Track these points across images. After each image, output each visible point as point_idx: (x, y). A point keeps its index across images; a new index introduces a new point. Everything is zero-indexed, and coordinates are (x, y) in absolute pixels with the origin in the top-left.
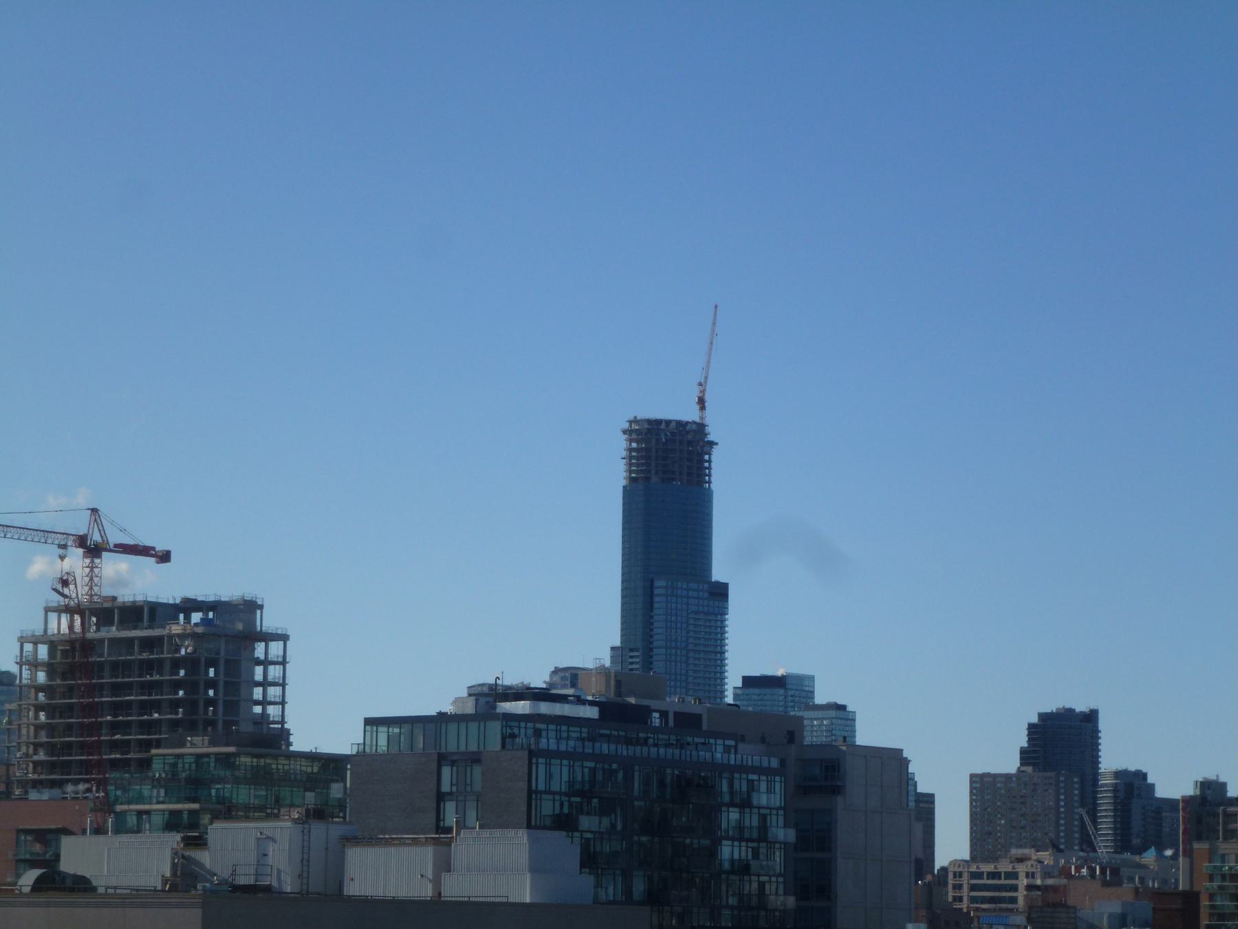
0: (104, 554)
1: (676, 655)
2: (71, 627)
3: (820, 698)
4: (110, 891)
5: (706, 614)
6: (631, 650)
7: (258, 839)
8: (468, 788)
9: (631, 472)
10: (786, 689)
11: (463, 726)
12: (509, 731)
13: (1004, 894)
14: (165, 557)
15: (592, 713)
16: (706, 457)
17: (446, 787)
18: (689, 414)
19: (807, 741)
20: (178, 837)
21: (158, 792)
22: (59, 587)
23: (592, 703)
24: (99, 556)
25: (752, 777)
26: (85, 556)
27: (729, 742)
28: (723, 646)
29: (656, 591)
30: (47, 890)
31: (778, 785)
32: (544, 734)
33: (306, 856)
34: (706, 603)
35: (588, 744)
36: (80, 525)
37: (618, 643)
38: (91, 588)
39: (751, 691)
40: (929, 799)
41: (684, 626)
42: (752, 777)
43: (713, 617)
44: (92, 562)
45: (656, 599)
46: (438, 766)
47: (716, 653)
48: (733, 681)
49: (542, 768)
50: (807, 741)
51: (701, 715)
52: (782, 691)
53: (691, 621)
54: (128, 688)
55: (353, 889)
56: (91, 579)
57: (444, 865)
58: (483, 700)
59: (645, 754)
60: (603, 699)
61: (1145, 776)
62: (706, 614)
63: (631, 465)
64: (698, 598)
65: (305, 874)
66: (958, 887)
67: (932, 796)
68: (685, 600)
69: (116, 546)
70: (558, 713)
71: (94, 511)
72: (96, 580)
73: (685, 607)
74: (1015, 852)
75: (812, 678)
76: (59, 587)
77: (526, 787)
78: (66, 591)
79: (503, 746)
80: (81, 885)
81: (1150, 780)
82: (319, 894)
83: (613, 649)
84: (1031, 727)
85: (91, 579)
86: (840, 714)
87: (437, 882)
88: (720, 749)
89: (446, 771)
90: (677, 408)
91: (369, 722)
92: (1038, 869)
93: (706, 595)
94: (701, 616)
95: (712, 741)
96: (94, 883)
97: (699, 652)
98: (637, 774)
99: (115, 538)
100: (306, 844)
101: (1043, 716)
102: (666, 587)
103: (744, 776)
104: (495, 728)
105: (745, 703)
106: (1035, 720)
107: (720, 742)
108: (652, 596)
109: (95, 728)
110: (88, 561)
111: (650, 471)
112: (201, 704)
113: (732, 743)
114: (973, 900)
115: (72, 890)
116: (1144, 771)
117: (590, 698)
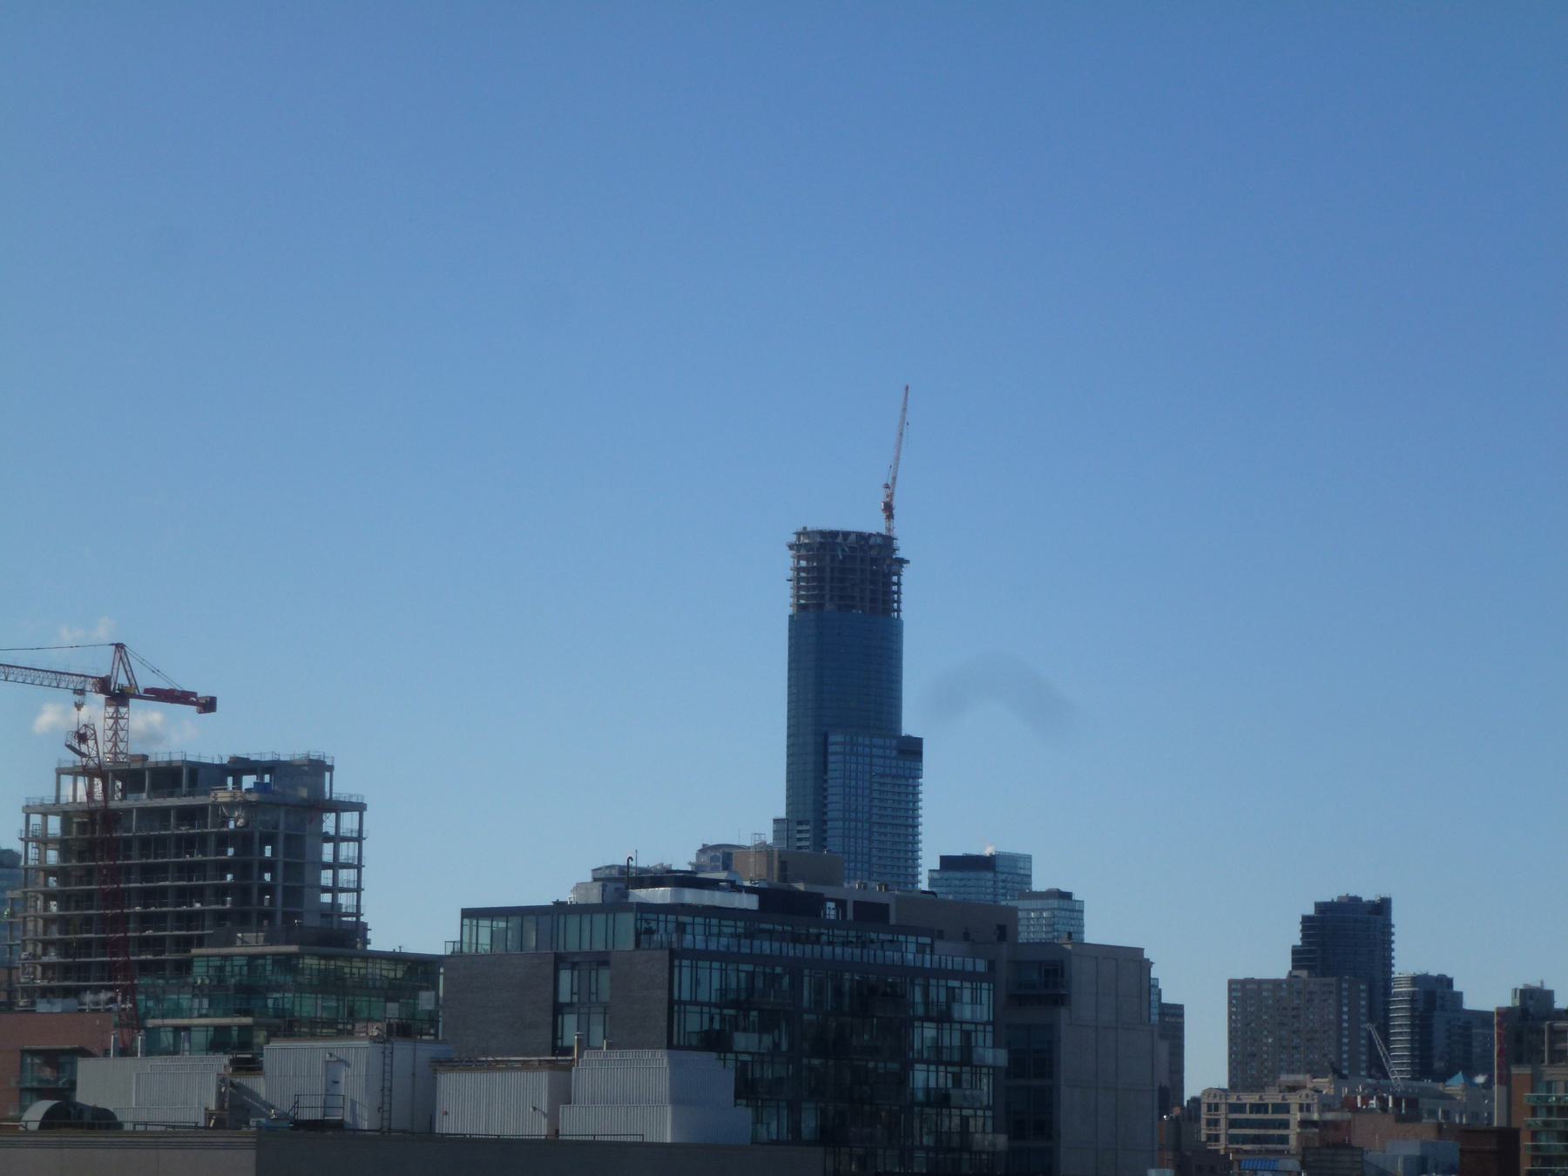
0: (132, 701)
1: (856, 829)
2: (90, 794)
3: (1039, 884)
4: (139, 1128)
5: (894, 777)
6: (800, 823)
7: (327, 1062)
8: (593, 998)
9: (799, 597)
10: (995, 872)
11: (586, 919)
12: (645, 925)
13: (1271, 1132)
14: (209, 705)
15: (750, 902)
16: (895, 579)
17: (564, 997)
18: (873, 524)
19: (1023, 937)
20: (225, 1059)
21: (201, 1003)
22: (75, 743)
23: (749, 890)
24: (126, 704)
25: (953, 983)
26: (108, 704)
27: (923, 940)
28: (915, 817)
29: (831, 749)
30: (60, 1126)
31: (985, 994)
32: (689, 929)
33: (387, 1084)
34: (894, 763)
35: (745, 942)
36: (102, 665)
37: (782, 814)
38: (115, 745)
39: (951, 874)
40: (1177, 1012)
41: (867, 792)
42: (953, 983)
43: (903, 782)
44: (117, 711)
45: (831, 758)
46: (554, 969)
47: (907, 826)
48: (928, 862)
49: (686, 973)
50: (1023, 937)
51: (887, 905)
52: (990, 875)
53: (876, 787)
54: (162, 870)
55: (447, 1125)
56: (116, 733)
57: (563, 1096)
58: (611, 886)
59: (817, 955)
60: (764, 885)
61: (1450, 982)
62: (894, 777)
63: (799, 588)
64: (884, 757)
65: (386, 1107)
66: (1213, 1123)
67: (1181, 1007)
68: (867, 760)
69: (147, 691)
70: (707, 903)
71: (119, 647)
72: (121, 734)
73: (867, 768)
74: (1285, 1078)
75: (1028, 859)
76: (75, 743)
77: (666, 997)
78: (84, 748)
79: (638, 944)
80: (103, 1121)
81: (1456, 988)
82: (404, 1131)
83: (776, 821)
84: (1306, 920)
85: (116, 733)
86: (1064, 903)
87: (553, 1116)
88: (912, 948)
89: (565, 976)
90: (858, 516)
91: (467, 914)
92: (1314, 1100)
93: (894, 753)
94: (888, 780)
95: (902, 938)
96: (120, 1118)
97: (885, 825)
98: (806, 979)
99: (145, 681)
100: (388, 1069)
101: (1321, 907)
102: (844, 744)
103: (942, 982)
104: (627, 922)
105: (944, 890)
106: (1311, 911)
107: (912, 939)
108: (825, 754)
109: (121, 922)
110: (111, 710)
111: (823, 597)
112: (255, 891)
113: (927, 940)
114: (1232, 1139)
115: (91, 1127)
116: (1449, 975)
117: (747, 884)
